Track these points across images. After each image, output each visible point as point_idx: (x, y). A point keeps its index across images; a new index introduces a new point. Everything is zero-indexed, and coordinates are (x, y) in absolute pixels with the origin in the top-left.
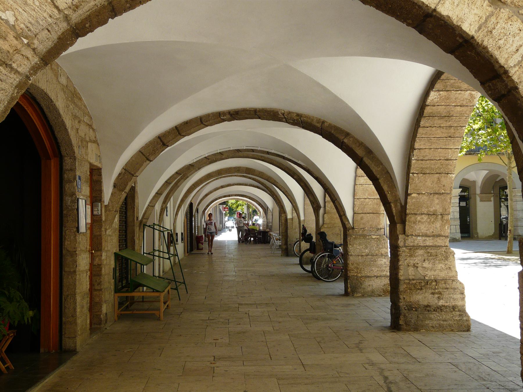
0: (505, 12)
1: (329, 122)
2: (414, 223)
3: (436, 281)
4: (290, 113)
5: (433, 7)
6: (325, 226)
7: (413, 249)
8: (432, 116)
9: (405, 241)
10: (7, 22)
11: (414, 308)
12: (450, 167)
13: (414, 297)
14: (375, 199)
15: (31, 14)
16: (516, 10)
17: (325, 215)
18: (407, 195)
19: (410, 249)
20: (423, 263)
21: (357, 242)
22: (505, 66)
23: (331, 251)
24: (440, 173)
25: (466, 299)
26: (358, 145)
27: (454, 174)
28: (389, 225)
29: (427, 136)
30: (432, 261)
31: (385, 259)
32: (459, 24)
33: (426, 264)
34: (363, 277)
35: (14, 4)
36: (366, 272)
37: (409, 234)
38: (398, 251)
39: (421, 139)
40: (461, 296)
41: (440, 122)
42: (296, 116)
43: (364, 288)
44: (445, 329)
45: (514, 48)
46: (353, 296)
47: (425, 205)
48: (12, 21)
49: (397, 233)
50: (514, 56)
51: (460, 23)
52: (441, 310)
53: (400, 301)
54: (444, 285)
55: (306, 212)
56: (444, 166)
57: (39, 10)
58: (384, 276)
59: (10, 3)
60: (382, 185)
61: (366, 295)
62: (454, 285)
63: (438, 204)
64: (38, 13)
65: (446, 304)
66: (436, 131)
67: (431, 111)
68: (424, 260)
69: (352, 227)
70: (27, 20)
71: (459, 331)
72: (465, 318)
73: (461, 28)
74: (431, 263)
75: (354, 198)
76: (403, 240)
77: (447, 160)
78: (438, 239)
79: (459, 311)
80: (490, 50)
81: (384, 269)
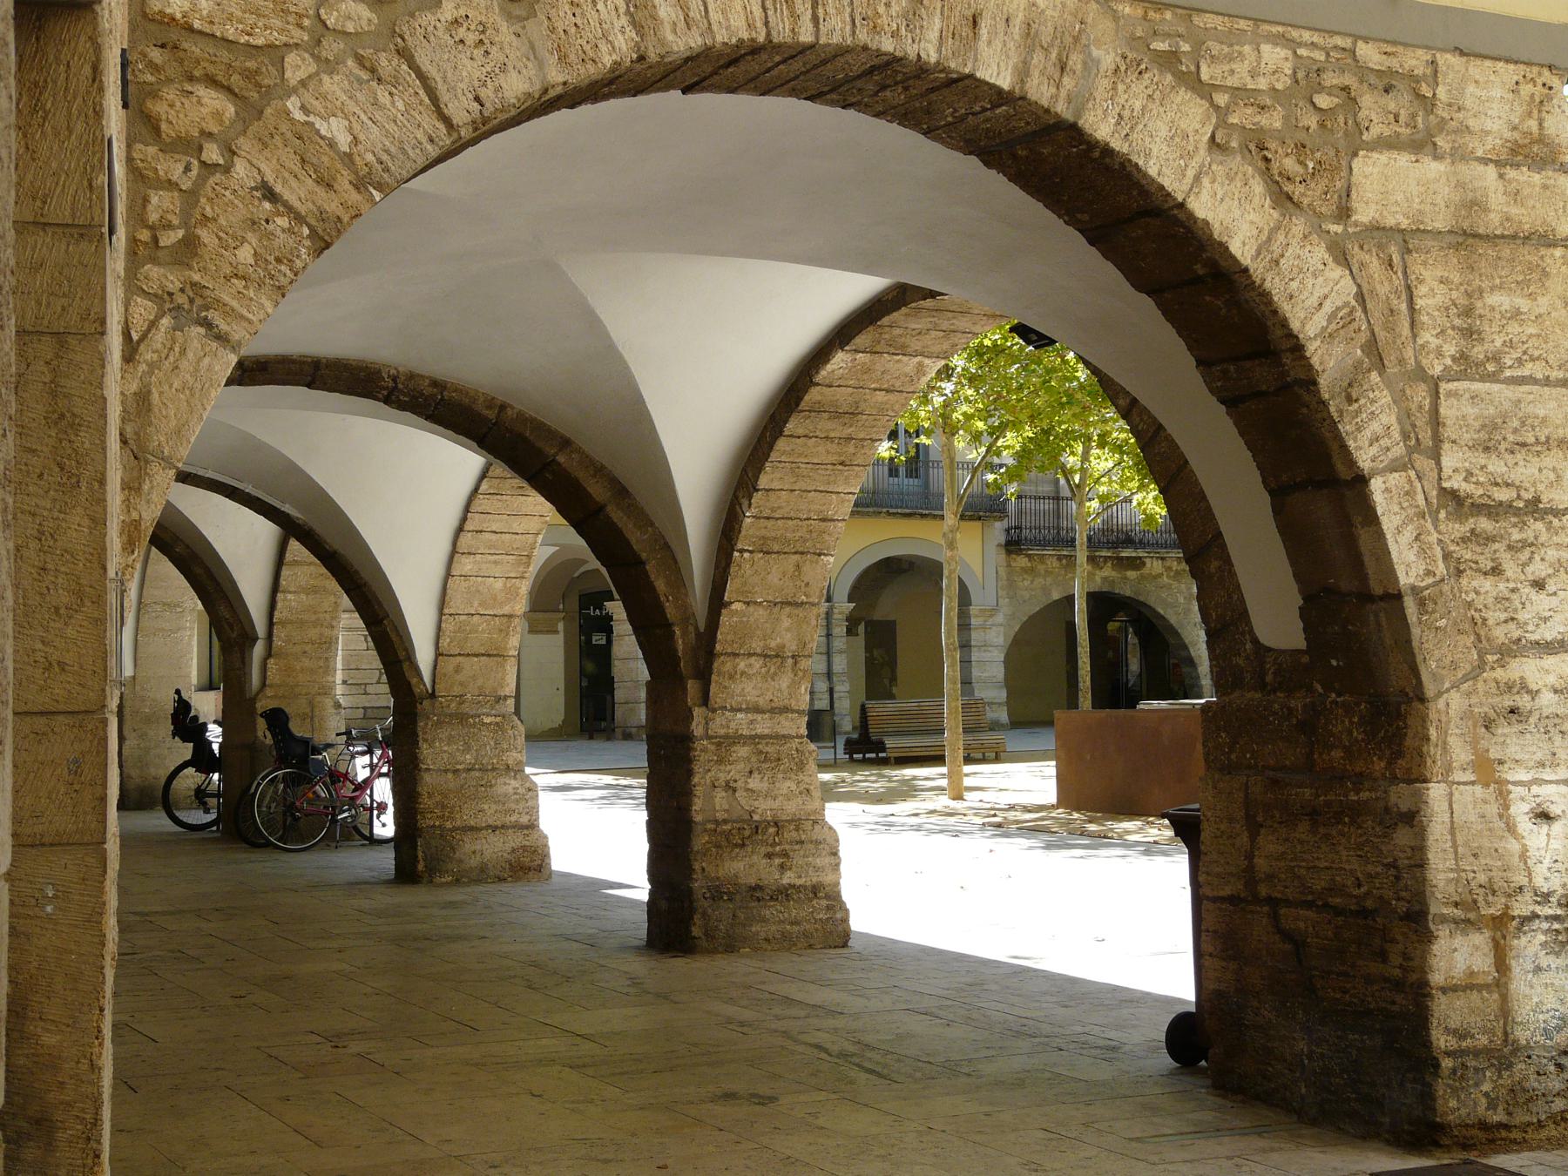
0: (1299, 225)
1: (518, 407)
2: (731, 677)
3: (776, 823)
4: (412, 376)
5: (1180, 200)
6: (269, 692)
7: (727, 742)
8: (817, 410)
9: (707, 723)
10: (332, 144)
11: (725, 893)
12: (826, 537)
13: (727, 865)
14: (496, 616)
15: (387, 131)
16: (1315, 220)
17: (271, 661)
18: (717, 602)
19: (719, 744)
20: (749, 780)
21: (444, 733)
22: (1301, 336)
23: (303, 762)
24: (802, 553)
25: (842, 867)
26: (592, 472)
27: (832, 556)
28: (648, 684)
29: (791, 460)
30: (769, 774)
31: (515, 778)
32: (1225, 239)
33: (755, 783)
34: (458, 829)
35: (348, 102)
36: (467, 817)
37: (716, 706)
38: (690, 749)
39: (779, 465)
40: (832, 860)
41: (830, 425)
42: (429, 386)
43: (461, 861)
44: (795, 945)
45: (1314, 301)
46: (431, 882)
47: (758, 632)
48: (344, 142)
49: (686, 702)
50: (1315, 317)
51: (1226, 238)
52: (787, 895)
53: (695, 877)
54: (794, 834)
55: (139, 655)
56: (814, 535)
57: (406, 122)
58: (514, 827)
59: (340, 100)
60: (653, 577)
61: (466, 880)
62: (817, 833)
63: (788, 630)
64: (404, 130)
65: (799, 882)
66: (814, 447)
67: (820, 398)
68: (751, 772)
69: (430, 691)
70: (380, 145)
71: (825, 948)
72: (839, 916)
73: (1227, 248)
74: (766, 778)
75: (441, 613)
76: (704, 722)
77: (823, 520)
78: (782, 718)
79: (827, 897)
80: (1276, 299)
81: (513, 806)
